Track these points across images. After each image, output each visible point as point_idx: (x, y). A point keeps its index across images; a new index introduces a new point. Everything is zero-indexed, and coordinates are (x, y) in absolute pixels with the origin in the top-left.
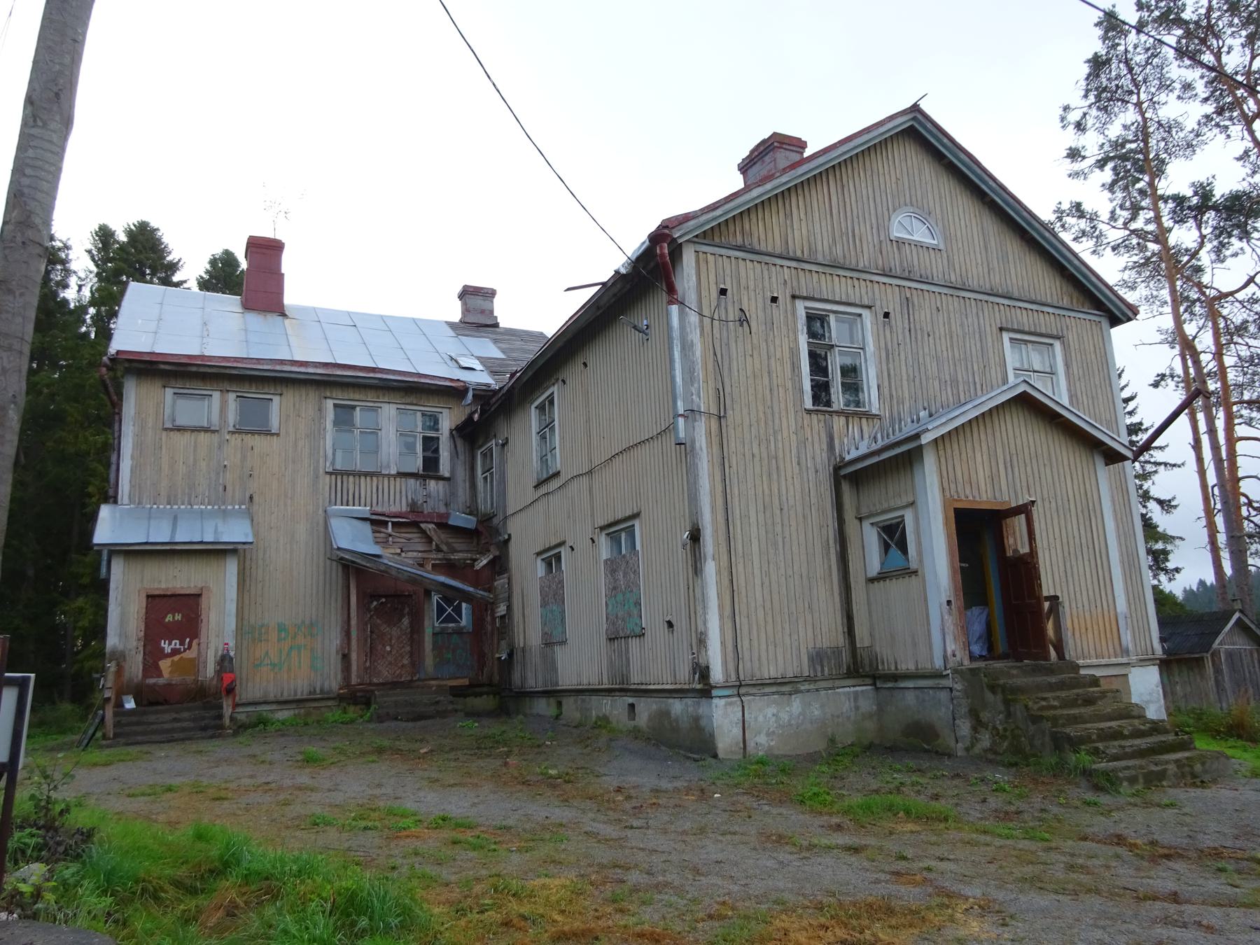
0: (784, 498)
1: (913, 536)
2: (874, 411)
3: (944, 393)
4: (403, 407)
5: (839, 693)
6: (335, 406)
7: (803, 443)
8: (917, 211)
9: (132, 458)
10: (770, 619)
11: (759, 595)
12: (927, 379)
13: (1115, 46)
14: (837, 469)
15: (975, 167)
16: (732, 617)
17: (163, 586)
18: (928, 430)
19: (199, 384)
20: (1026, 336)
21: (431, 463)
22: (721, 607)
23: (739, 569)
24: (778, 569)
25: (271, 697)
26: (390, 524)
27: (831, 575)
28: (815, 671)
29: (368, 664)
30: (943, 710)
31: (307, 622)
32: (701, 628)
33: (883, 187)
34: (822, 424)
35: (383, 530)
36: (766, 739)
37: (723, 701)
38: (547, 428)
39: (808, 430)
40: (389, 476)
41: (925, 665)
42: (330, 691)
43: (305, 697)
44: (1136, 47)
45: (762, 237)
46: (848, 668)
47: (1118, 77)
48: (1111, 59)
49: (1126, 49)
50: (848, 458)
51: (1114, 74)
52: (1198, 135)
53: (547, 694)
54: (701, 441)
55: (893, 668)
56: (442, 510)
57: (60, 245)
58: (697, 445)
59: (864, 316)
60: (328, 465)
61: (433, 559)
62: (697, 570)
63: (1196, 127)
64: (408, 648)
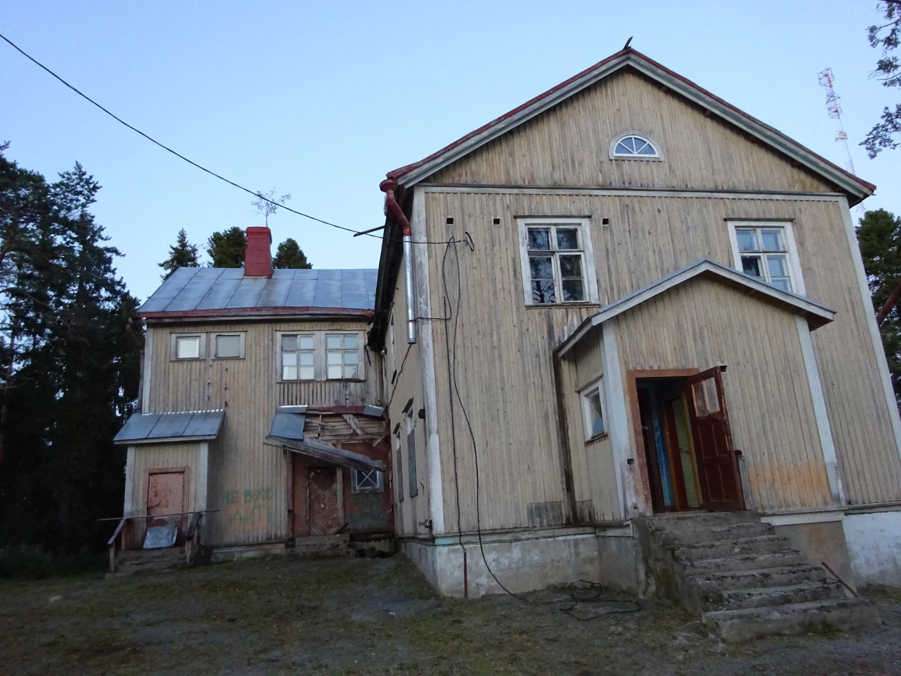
4: (330, 332)
5: (559, 541)
6: (283, 335)
15: (691, 88)
16: (453, 479)
17: (160, 467)
19: (191, 329)
26: (321, 416)
27: (549, 441)
28: (533, 522)
29: (308, 518)
31: (265, 488)
37: (446, 549)
40: (321, 381)
42: (280, 538)
43: (264, 542)
46: (568, 519)
55: (602, 519)
56: (360, 404)
57: (190, 249)
59: (583, 224)
60: (278, 377)
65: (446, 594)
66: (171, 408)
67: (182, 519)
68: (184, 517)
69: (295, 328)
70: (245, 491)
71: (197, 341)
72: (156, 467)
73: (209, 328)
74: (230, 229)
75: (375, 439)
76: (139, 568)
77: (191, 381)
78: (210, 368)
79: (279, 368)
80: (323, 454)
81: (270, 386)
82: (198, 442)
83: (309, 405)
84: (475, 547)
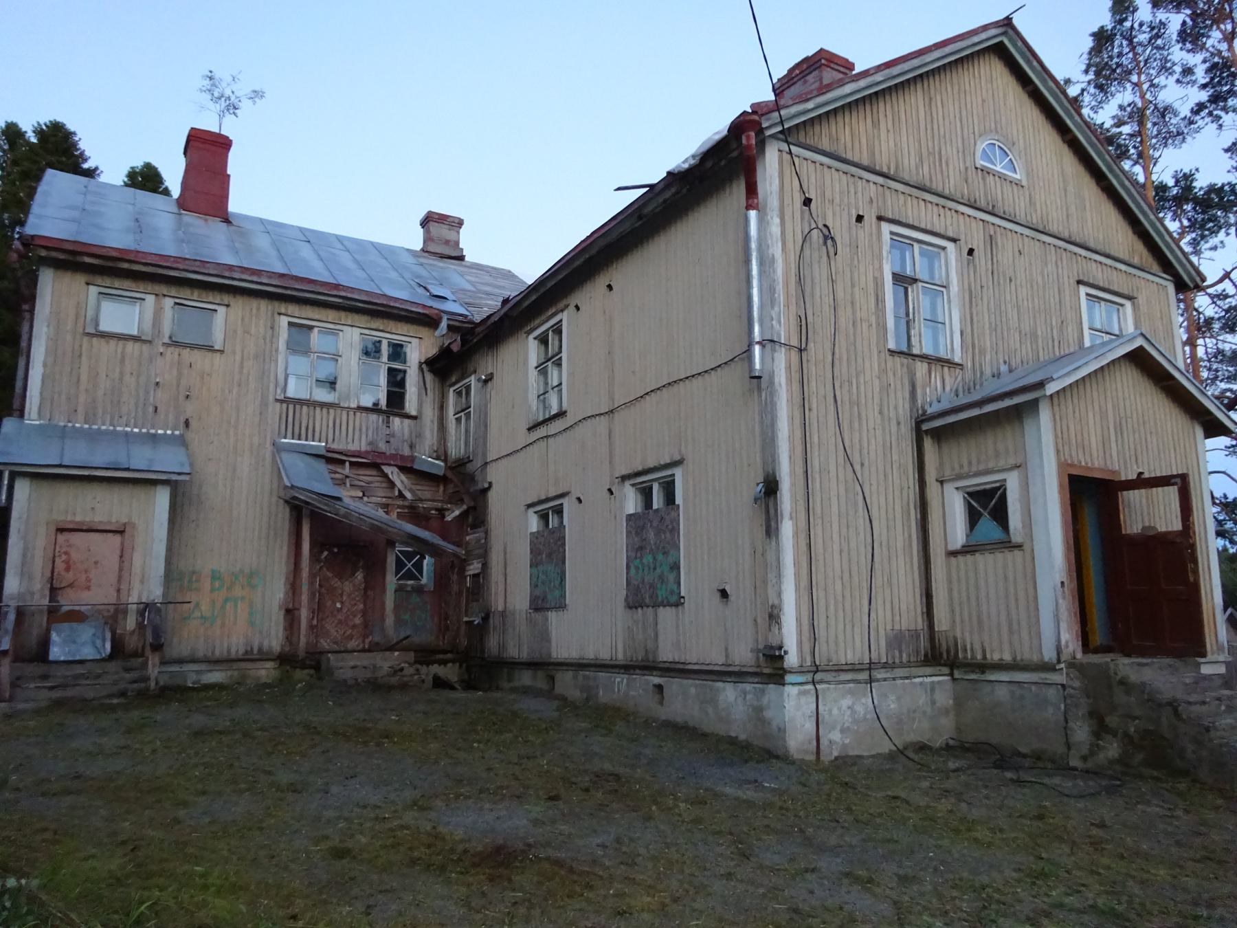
0: (865, 451)
1: (1018, 506)
2: (957, 359)
3: (1024, 346)
6: (290, 324)
7: (886, 388)
8: (1001, 139)
9: (45, 365)
10: (848, 594)
11: (837, 564)
12: (1009, 329)
13: (1121, 22)
14: (918, 423)
16: (809, 588)
17: (78, 519)
18: (1052, 379)
19: (127, 284)
20: (1104, 292)
21: (396, 398)
22: (797, 575)
23: (817, 532)
24: (858, 534)
25: (200, 654)
26: (347, 464)
29: (315, 622)
30: (1051, 710)
32: (773, 599)
33: (969, 106)
34: (905, 369)
35: (339, 470)
36: (839, 735)
38: (552, 359)
39: (890, 374)
41: (1027, 655)
43: (241, 657)
44: (1141, 25)
45: (849, 145)
46: (926, 655)
47: (1120, 55)
48: (1115, 35)
49: (1132, 26)
50: (930, 411)
51: (1116, 50)
52: (1191, 123)
53: (534, 665)
54: (781, 378)
56: (406, 452)
58: (776, 380)
60: (279, 391)
61: (399, 507)
62: (771, 530)
63: (1189, 115)
64: (361, 606)
65: (796, 756)
66: (81, 417)
67: (117, 611)
68: (119, 611)
69: (311, 315)
70: (213, 571)
71: (137, 307)
72: (69, 518)
73: (163, 289)
74: (48, 124)
75: (448, 510)
76: (56, 694)
77: (122, 374)
78: (159, 359)
79: (281, 377)
80: (373, 524)
81: (264, 404)
82: (154, 483)
83: (327, 443)
84: (828, 689)
